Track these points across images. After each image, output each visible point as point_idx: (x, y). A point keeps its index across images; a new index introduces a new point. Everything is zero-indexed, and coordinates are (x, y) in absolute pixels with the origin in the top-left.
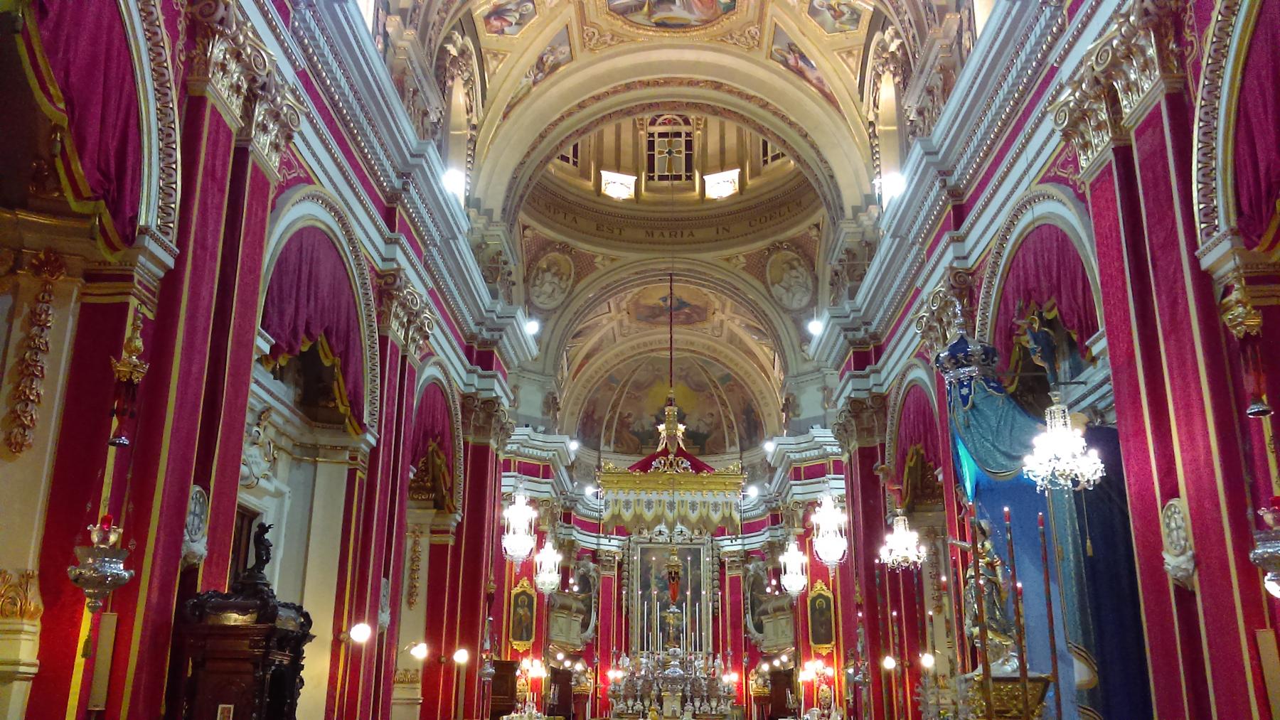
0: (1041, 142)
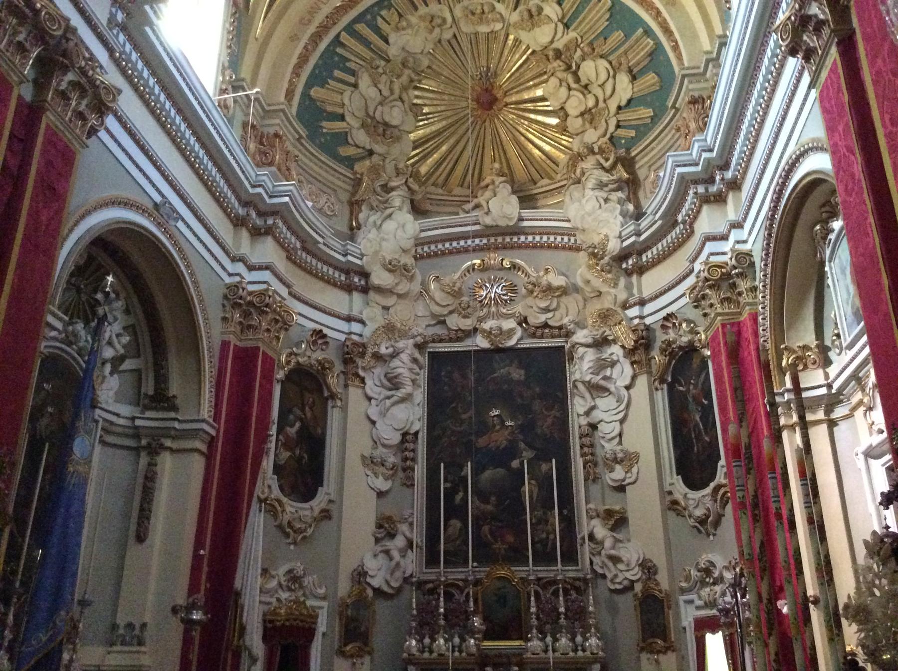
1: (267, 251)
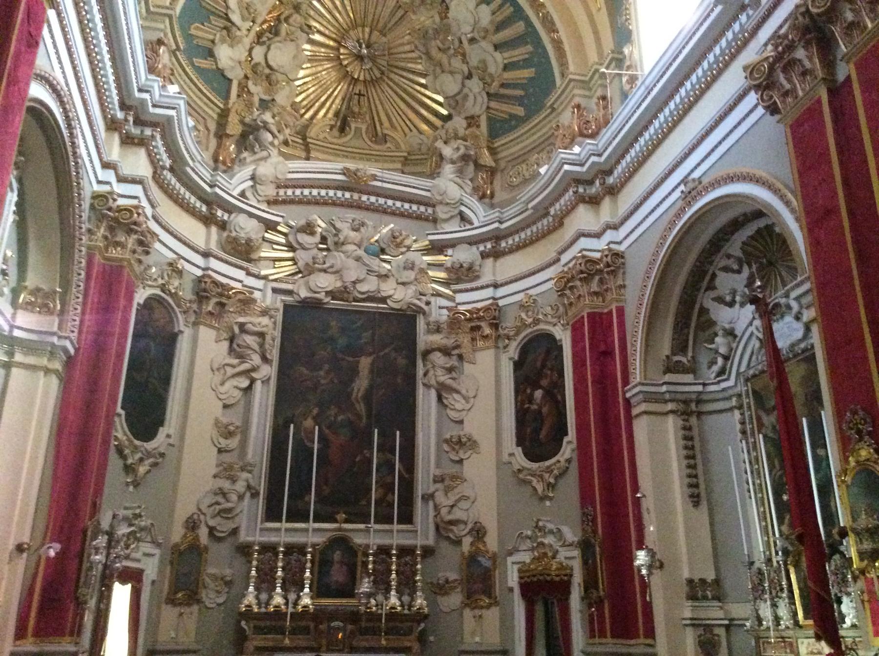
0: (740, 128)
1: (137, 163)
